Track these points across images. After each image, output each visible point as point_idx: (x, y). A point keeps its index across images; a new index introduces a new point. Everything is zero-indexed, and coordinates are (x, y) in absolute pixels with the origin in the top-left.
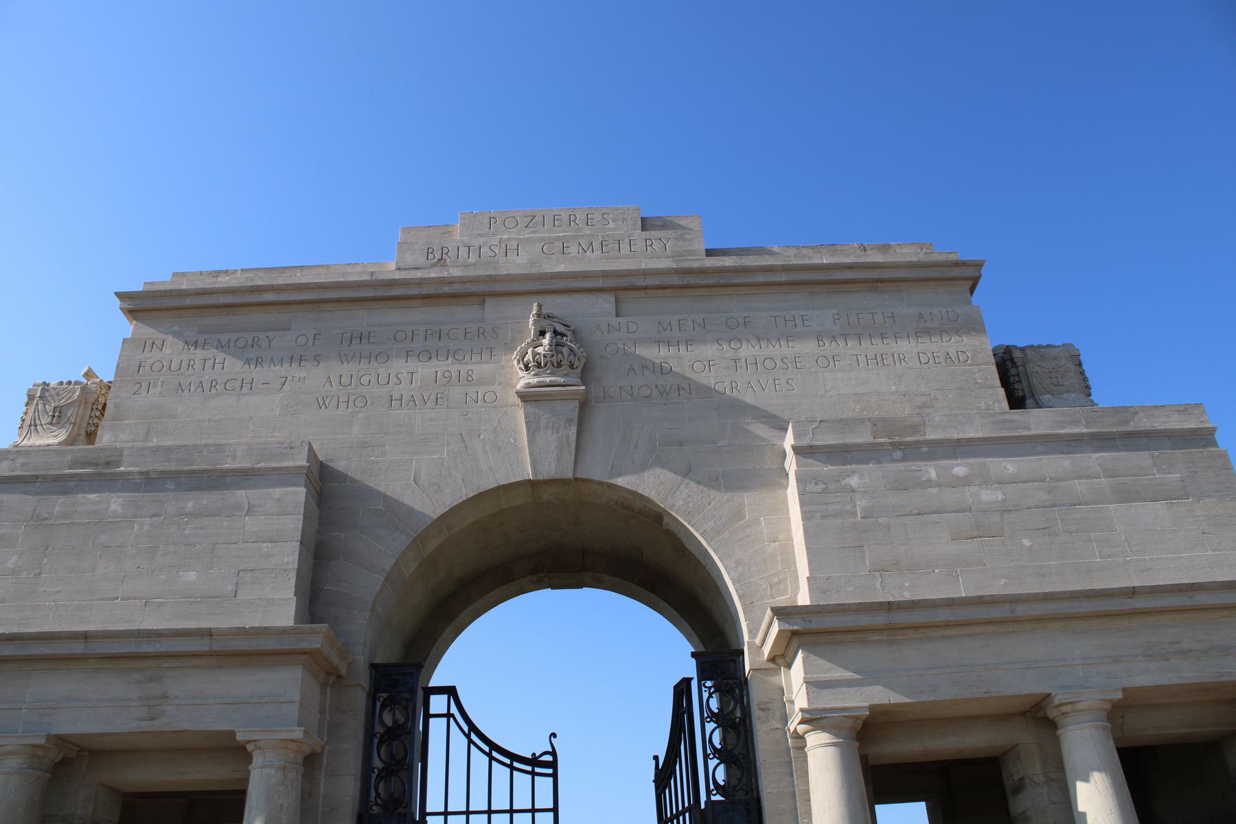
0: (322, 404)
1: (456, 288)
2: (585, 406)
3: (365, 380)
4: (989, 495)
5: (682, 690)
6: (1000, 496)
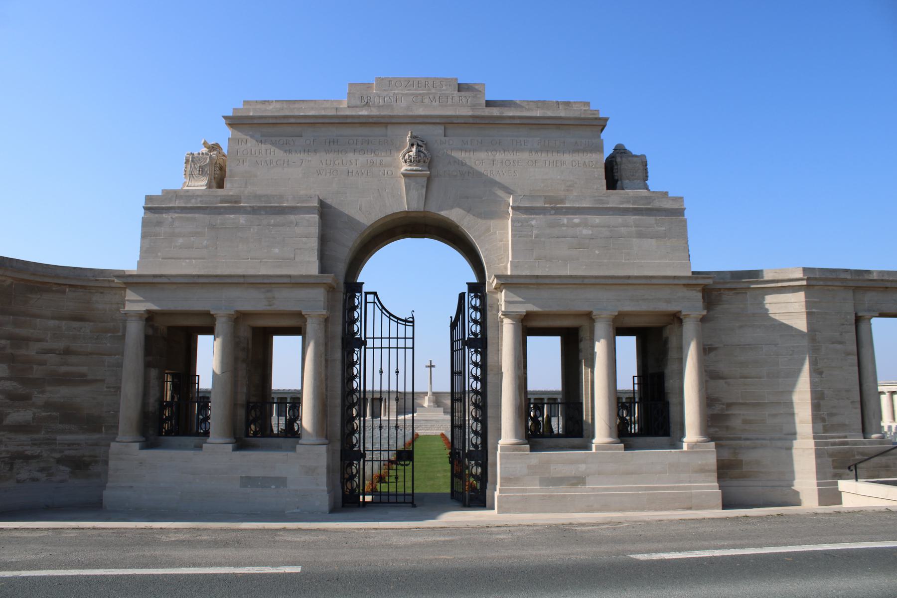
0: (319, 173)
1: (375, 120)
2: (429, 179)
3: (337, 162)
4: (586, 232)
5: (462, 296)
6: (590, 232)
